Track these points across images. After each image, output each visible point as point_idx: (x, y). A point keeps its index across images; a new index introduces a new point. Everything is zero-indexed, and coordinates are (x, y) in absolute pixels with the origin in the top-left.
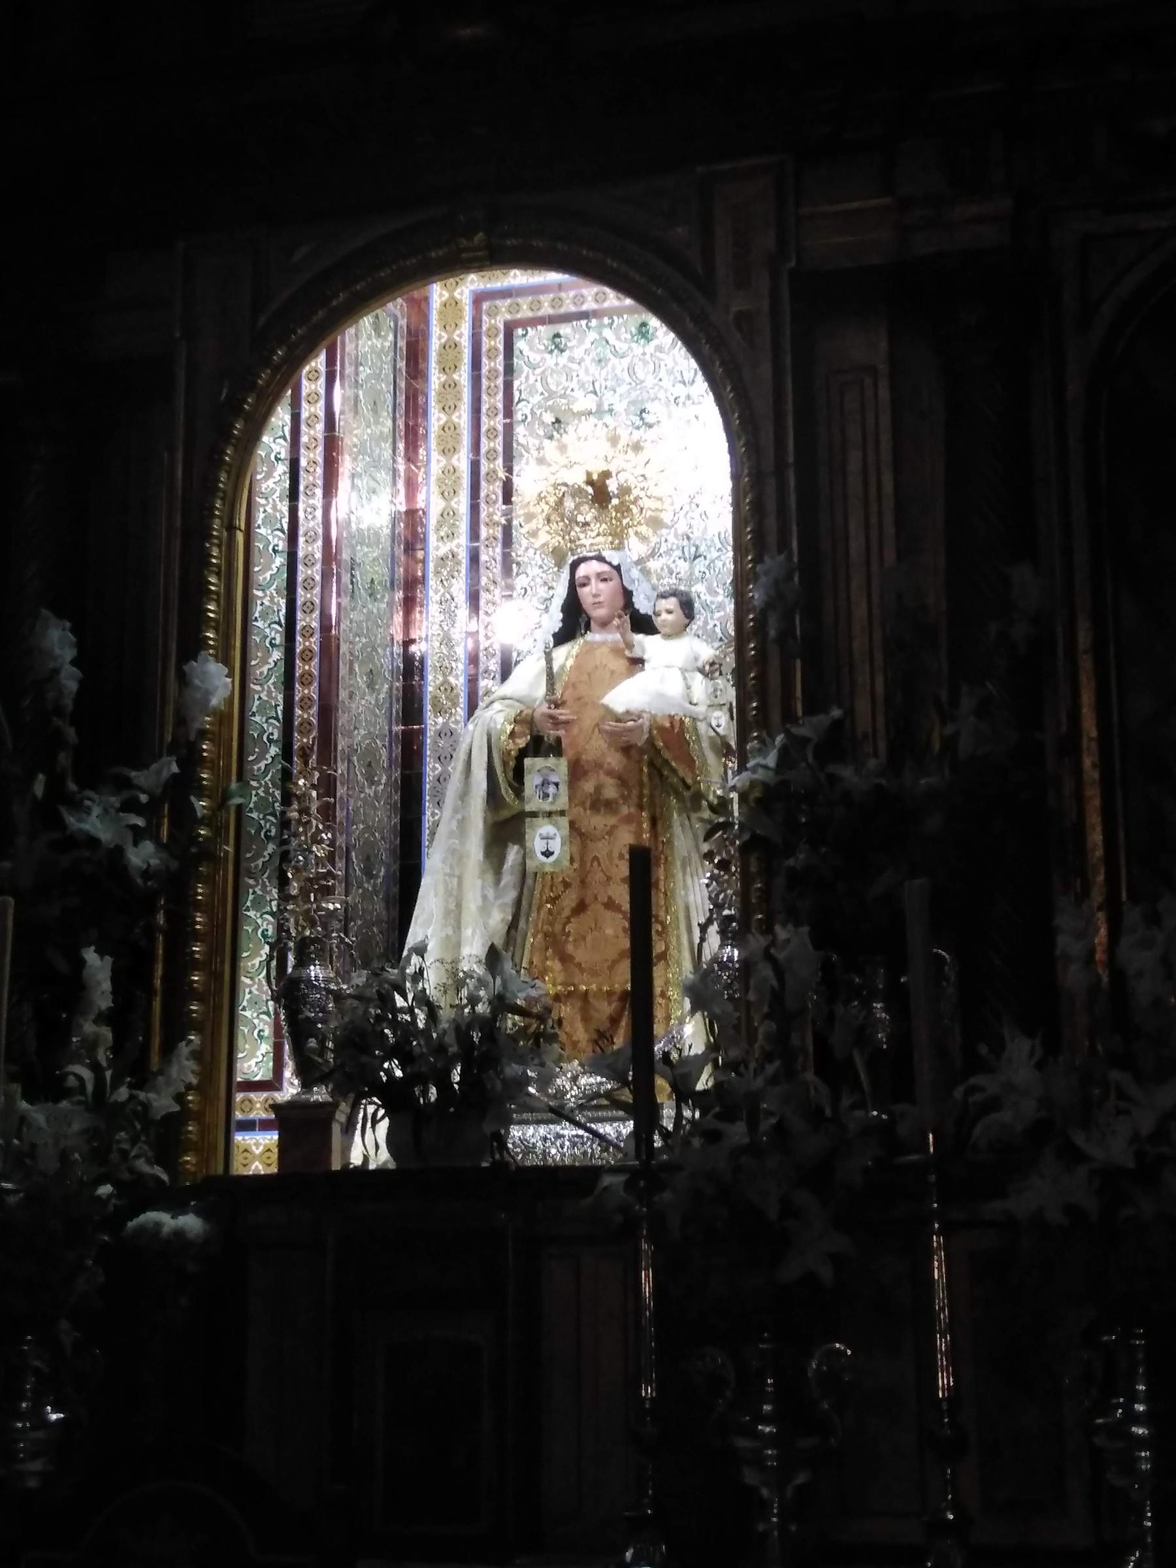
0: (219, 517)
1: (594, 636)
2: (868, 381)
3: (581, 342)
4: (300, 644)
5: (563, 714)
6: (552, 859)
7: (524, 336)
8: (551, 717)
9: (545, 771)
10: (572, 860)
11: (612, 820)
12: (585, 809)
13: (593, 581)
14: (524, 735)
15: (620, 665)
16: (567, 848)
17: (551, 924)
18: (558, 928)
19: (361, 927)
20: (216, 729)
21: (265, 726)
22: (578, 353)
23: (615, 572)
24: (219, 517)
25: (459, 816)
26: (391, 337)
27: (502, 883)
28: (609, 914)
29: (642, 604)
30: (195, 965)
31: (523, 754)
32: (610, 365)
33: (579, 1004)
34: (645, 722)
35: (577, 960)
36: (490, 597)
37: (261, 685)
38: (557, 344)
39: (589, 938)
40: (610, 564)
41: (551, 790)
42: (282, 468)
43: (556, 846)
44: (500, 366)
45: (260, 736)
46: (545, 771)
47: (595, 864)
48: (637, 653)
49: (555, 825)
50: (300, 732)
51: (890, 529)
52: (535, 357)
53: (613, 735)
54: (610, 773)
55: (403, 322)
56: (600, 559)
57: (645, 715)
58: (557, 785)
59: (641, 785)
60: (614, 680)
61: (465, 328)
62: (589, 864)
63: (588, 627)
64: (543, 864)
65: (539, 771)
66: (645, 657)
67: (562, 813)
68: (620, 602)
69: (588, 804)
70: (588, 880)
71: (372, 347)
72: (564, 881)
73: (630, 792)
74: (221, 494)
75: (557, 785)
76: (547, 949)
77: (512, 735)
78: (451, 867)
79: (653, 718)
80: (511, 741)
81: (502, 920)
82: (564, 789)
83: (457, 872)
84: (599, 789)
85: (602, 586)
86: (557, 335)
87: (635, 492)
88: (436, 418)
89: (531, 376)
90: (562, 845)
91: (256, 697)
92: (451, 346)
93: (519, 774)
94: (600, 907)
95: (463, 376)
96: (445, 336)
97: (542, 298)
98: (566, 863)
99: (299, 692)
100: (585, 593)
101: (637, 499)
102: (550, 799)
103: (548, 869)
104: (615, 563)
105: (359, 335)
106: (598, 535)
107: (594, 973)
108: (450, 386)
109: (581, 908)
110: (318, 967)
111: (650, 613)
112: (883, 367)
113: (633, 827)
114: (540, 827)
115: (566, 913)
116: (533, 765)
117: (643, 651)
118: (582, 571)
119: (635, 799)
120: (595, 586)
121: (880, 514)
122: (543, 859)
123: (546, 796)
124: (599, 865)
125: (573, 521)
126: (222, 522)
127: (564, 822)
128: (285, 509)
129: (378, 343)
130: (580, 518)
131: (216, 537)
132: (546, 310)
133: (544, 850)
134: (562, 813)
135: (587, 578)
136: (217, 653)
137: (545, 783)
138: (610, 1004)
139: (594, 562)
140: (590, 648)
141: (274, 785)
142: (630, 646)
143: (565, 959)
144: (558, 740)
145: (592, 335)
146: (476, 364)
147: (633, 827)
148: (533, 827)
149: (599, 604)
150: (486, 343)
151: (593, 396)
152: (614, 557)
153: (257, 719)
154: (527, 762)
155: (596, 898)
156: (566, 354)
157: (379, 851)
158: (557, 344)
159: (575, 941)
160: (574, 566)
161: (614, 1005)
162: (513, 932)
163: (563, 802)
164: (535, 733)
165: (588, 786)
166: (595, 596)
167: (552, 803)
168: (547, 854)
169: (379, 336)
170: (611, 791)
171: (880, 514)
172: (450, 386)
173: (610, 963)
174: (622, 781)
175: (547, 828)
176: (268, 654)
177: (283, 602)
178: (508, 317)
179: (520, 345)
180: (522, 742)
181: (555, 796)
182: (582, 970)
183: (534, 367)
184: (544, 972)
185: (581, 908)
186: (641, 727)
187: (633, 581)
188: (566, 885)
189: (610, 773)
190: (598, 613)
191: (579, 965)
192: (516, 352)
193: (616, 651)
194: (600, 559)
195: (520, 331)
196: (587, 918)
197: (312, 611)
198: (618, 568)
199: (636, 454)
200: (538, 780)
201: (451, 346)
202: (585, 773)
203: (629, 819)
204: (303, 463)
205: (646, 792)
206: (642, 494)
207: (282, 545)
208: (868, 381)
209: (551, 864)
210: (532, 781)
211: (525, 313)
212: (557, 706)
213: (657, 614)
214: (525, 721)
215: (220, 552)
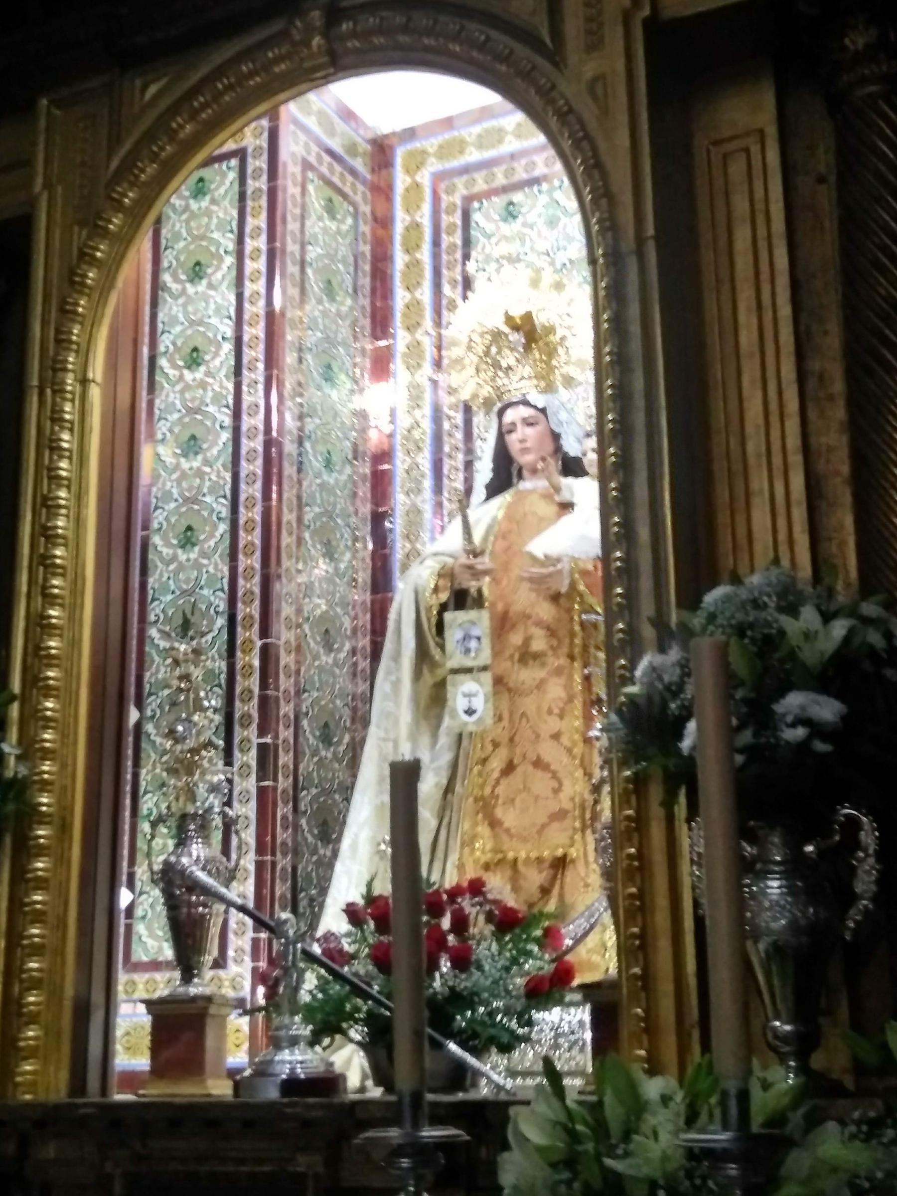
0: (73, 371)
1: (526, 485)
2: (755, 149)
3: (533, 206)
4: (244, 515)
5: (485, 562)
6: (475, 717)
7: (480, 209)
8: (470, 567)
9: (466, 625)
10: (500, 719)
11: (540, 674)
12: (513, 664)
13: (519, 426)
14: (445, 589)
15: (548, 509)
16: (490, 705)
17: (482, 787)
18: (488, 791)
19: (315, 798)
20: (66, 593)
21: (212, 598)
22: (531, 218)
23: (541, 416)
24: (73, 371)
25: (393, 678)
26: (350, 221)
27: (438, 747)
28: (539, 774)
29: (571, 447)
30: (41, 851)
31: (443, 608)
32: (561, 225)
33: (509, 873)
34: (565, 566)
35: (507, 824)
36: (453, 463)
37: (209, 559)
38: (510, 213)
39: (518, 801)
40: (535, 407)
41: (473, 644)
42: (228, 347)
43: (479, 703)
44: (458, 239)
45: (208, 608)
46: (466, 625)
47: (524, 720)
48: (565, 496)
49: (478, 681)
50: (244, 603)
51: (785, 310)
52: (489, 227)
53: (537, 581)
54: (539, 624)
55: (366, 209)
56: (526, 403)
57: (565, 559)
58: (479, 639)
59: (572, 635)
60: (543, 524)
61: (426, 208)
62: (518, 721)
63: (520, 477)
64: (466, 724)
65: (460, 625)
66: (575, 500)
67: (485, 668)
68: (549, 447)
69: (517, 656)
70: (517, 739)
71: (325, 230)
72: (493, 741)
73: (559, 641)
74: (74, 347)
75: (479, 639)
76: (478, 813)
77: (436, 590)
78: (386, 730)
79: (574, 559)
80: (434, 596)
81: (437, 785)
82: (486, 643)
83: (392, 736)
84: (527, 641)
85: (529, 431)
86: (511, 203)
87: (560, 333)
88: (401, 297)
89: (487, 245)
90: (486, 701)
91: (205, 570)
92: (414, 227)
93: (440, 628)
94: (530, 768)
95: (425, 255)
96: (408, 218)
97: (495, 170)
98: (489, 721)
99: (243, 562)
100: (512, 440)
101: (563, 339)
102: (473, 654)
103: (471, 728)
104: (540, 406)
105: (306, 215)
106: (522, 378)
107: (524, 839)
108: (414, 265)
109: (509, 769)
110: (200, 845)
111: (580, 455)
112: (772, 131)
113: (562, 680)
114: (462, 684)
115: (496, 775)
116: (455, 620)
117: (572, 495)
118: (511, 416)
119: (565, 650)
120: (523, 431)
121: (773, 294)
122: (465, 718)
123: (467, 651)
124: (528, 721)
125: (496, 365)
126: (76, 376)
127: (487, 678)
128: (230, 386)
129: (333, 226)
130: (504, 364)
131: (71, 392)
132: (500, 180)
133: (466, 709)
134: (485, 668)
135: (513, 424)
136: (69, 512)
137: (467, 637)
138: (540, 872)
139: (521, 407)
140: (522, 496)
141: (220, 657)
142: (557, 489)
143: (494, 823)
144: (480, 591)
145: (544, 199)
146: (436, 243)
147: (562, 680)
148: (454, 685)
149: (525, 451)
150: (445, 220)
151: (546, 257)
152: (540, 400)
153: (205, 592)
154: (448, 616)
155: (524, 756)
156: (520, 219)
157: (341, 718)
158: (510, 213)
159: (504, 804)
160: (501, 413)
161: (544, 874)
162: (449, 796)
163: (485, 656)
164: (457, 586)
165: (516, 639)
166: (522, 441)
167: (475, 658)
168: (470, 712)
169: (333, 217)
170: (539, 644)
171: (773, 294)
172: (414, 265)
173: (538, 827)
174: (552, 632)
175: (468, 685)
176: (215, 527)
177: (228, 476)
178: (465, 192)
179: (477, 217)
180: (444, 596)
181: (478, 651)
182: (511, 836)
183: (489, 237)
184: (474, 838)
185: (509, 769)
186: (560, 572)
187: (561, 423)
188: (496, 745)
189: (539, 624)
190: (525, 460)
191: (508, 831)
192: (473, 224)
193: (547, 497)
194: (526, 403)
195: (476, 205)
196: (516, 779)
197: (254, 482)
198: (543, 411)
199: (559, 293)
200: (459, 635)
201: (414, 227)
202: (513, 626)
203: (558, 671)
204: (246, 338)
205: (577, 641)
206: (567, 333)
207: (228, 421)
208: (755, 149)
209: (474, 723)
210: (453, 636)
211: (481, 185)
212: (476, 555)
213: (585, 454)
214: (446, 574)
215: (73, 407)
